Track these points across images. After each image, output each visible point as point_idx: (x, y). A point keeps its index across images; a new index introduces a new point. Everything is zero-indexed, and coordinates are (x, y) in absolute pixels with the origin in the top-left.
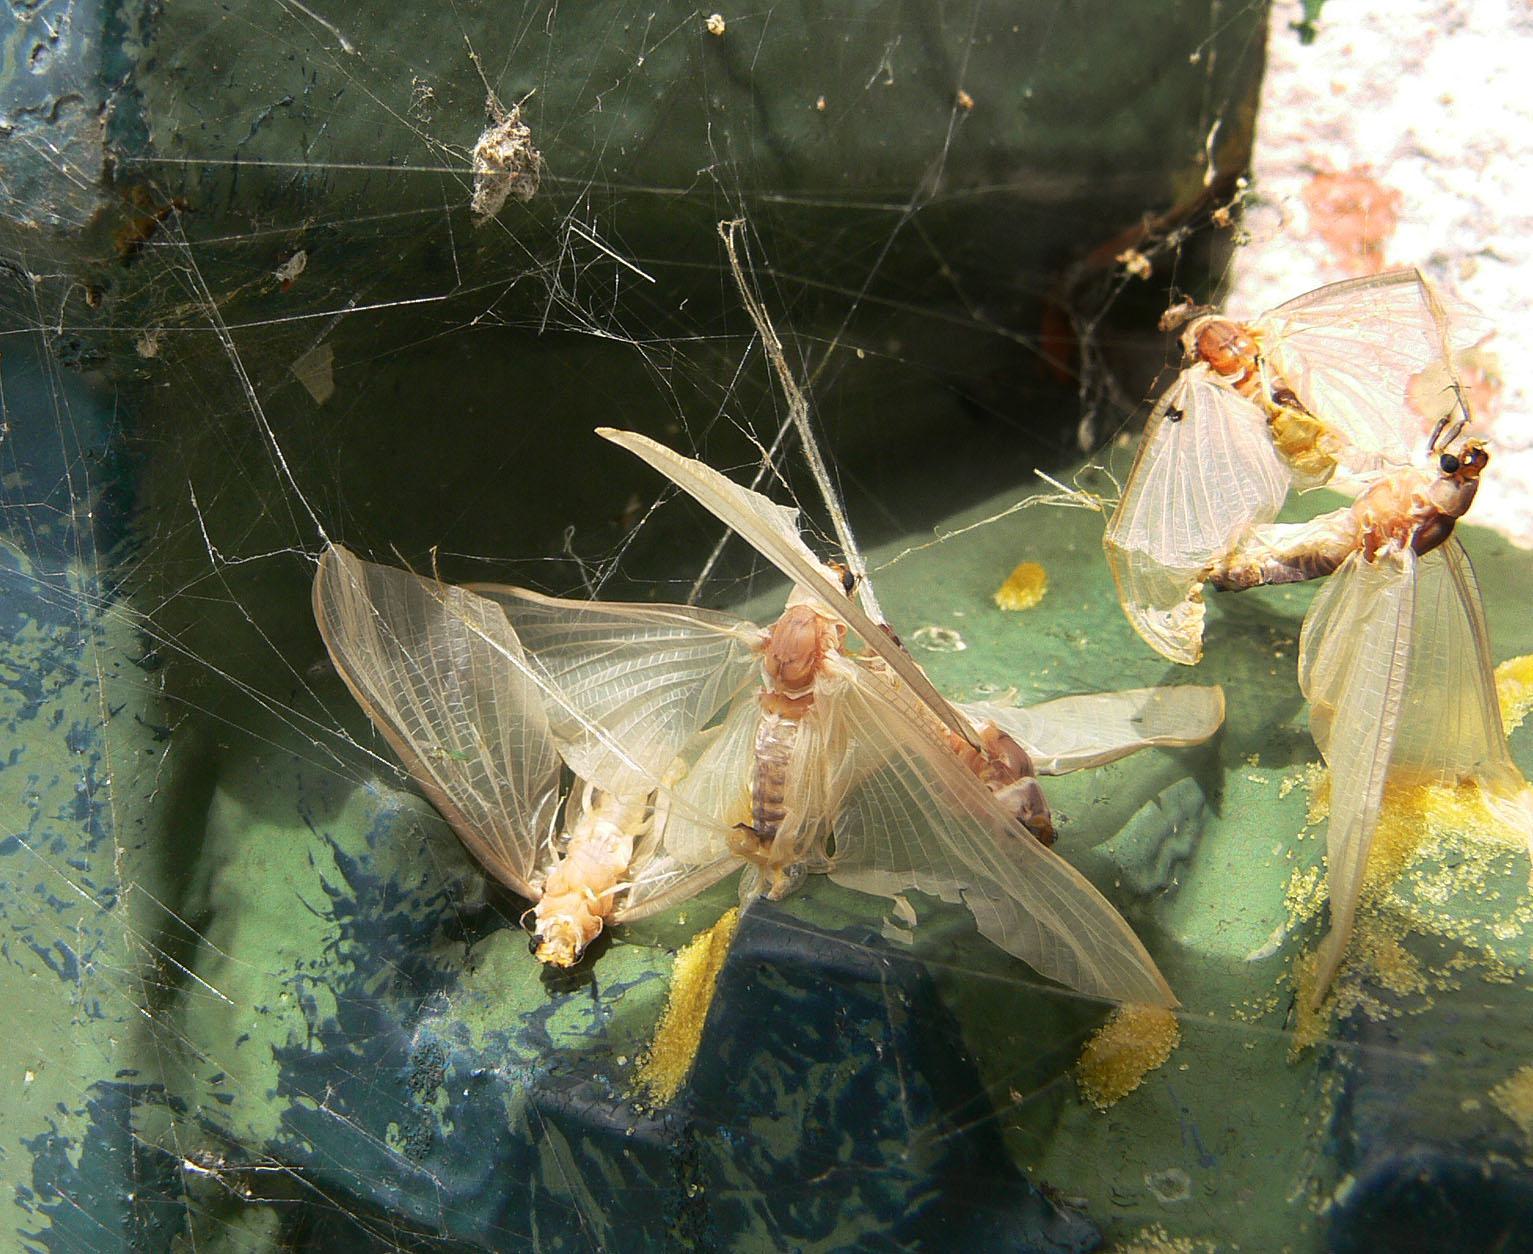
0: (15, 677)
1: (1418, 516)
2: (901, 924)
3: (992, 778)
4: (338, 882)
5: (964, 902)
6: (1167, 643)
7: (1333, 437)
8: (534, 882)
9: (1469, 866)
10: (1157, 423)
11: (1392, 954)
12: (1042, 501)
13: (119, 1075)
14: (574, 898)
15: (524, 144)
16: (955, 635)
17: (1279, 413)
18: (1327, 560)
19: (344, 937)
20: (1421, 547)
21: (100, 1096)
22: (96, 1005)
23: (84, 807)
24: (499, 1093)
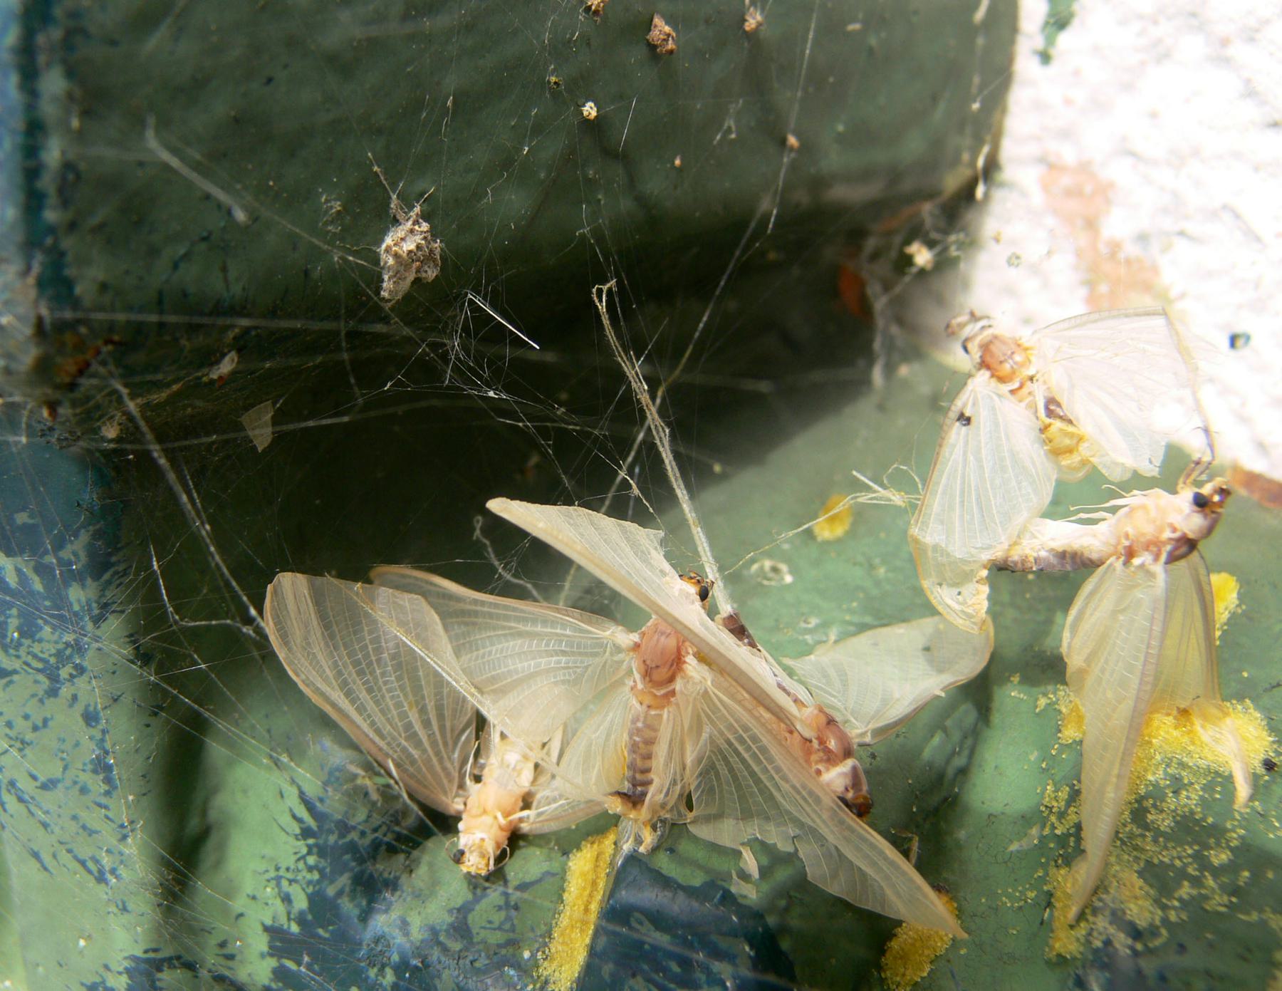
0: (40, 666)
2: (744, 876)
3: (821, 761)
4: (302, 812)
5: (797, 850)
8: (457, 800)
10: (950, 427)
11: (1133, 886)
12: (860, 500)
13: (146, 952)
14: (488, 820)
15: (425, 238)
16: (784, 567)
17: (1050, 425)
18: (1091, 561)
19: (309, 853)
21: (133, 965)
22: (124, 903)
23: (101, 767)
24: (432, 978)
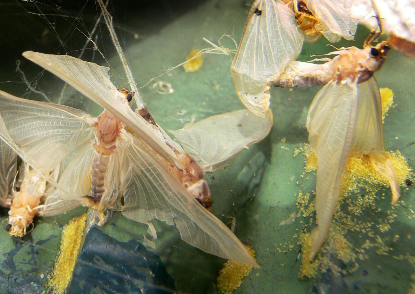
1: (360, 71)
2: (150, 237)
3: (187, 180)
5: (175, 224)
6: (255, 108)
7: (321, 24)
8: (8, 200)
9: (368, 195)
10: (251, 16)
11: (341, 242)
12: (207, 52)
14: (23, 209)
16: (169, 85)
17: (300, 15)
18: (321, 82)
20: (361, 81)
